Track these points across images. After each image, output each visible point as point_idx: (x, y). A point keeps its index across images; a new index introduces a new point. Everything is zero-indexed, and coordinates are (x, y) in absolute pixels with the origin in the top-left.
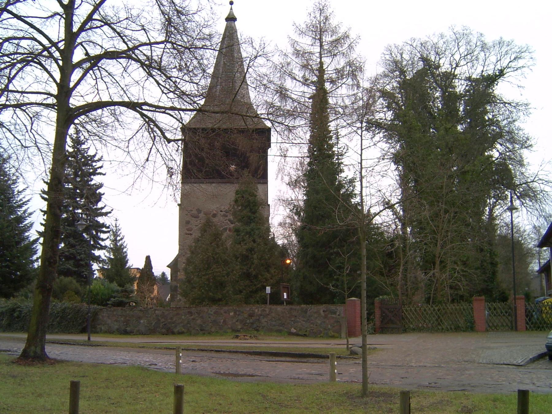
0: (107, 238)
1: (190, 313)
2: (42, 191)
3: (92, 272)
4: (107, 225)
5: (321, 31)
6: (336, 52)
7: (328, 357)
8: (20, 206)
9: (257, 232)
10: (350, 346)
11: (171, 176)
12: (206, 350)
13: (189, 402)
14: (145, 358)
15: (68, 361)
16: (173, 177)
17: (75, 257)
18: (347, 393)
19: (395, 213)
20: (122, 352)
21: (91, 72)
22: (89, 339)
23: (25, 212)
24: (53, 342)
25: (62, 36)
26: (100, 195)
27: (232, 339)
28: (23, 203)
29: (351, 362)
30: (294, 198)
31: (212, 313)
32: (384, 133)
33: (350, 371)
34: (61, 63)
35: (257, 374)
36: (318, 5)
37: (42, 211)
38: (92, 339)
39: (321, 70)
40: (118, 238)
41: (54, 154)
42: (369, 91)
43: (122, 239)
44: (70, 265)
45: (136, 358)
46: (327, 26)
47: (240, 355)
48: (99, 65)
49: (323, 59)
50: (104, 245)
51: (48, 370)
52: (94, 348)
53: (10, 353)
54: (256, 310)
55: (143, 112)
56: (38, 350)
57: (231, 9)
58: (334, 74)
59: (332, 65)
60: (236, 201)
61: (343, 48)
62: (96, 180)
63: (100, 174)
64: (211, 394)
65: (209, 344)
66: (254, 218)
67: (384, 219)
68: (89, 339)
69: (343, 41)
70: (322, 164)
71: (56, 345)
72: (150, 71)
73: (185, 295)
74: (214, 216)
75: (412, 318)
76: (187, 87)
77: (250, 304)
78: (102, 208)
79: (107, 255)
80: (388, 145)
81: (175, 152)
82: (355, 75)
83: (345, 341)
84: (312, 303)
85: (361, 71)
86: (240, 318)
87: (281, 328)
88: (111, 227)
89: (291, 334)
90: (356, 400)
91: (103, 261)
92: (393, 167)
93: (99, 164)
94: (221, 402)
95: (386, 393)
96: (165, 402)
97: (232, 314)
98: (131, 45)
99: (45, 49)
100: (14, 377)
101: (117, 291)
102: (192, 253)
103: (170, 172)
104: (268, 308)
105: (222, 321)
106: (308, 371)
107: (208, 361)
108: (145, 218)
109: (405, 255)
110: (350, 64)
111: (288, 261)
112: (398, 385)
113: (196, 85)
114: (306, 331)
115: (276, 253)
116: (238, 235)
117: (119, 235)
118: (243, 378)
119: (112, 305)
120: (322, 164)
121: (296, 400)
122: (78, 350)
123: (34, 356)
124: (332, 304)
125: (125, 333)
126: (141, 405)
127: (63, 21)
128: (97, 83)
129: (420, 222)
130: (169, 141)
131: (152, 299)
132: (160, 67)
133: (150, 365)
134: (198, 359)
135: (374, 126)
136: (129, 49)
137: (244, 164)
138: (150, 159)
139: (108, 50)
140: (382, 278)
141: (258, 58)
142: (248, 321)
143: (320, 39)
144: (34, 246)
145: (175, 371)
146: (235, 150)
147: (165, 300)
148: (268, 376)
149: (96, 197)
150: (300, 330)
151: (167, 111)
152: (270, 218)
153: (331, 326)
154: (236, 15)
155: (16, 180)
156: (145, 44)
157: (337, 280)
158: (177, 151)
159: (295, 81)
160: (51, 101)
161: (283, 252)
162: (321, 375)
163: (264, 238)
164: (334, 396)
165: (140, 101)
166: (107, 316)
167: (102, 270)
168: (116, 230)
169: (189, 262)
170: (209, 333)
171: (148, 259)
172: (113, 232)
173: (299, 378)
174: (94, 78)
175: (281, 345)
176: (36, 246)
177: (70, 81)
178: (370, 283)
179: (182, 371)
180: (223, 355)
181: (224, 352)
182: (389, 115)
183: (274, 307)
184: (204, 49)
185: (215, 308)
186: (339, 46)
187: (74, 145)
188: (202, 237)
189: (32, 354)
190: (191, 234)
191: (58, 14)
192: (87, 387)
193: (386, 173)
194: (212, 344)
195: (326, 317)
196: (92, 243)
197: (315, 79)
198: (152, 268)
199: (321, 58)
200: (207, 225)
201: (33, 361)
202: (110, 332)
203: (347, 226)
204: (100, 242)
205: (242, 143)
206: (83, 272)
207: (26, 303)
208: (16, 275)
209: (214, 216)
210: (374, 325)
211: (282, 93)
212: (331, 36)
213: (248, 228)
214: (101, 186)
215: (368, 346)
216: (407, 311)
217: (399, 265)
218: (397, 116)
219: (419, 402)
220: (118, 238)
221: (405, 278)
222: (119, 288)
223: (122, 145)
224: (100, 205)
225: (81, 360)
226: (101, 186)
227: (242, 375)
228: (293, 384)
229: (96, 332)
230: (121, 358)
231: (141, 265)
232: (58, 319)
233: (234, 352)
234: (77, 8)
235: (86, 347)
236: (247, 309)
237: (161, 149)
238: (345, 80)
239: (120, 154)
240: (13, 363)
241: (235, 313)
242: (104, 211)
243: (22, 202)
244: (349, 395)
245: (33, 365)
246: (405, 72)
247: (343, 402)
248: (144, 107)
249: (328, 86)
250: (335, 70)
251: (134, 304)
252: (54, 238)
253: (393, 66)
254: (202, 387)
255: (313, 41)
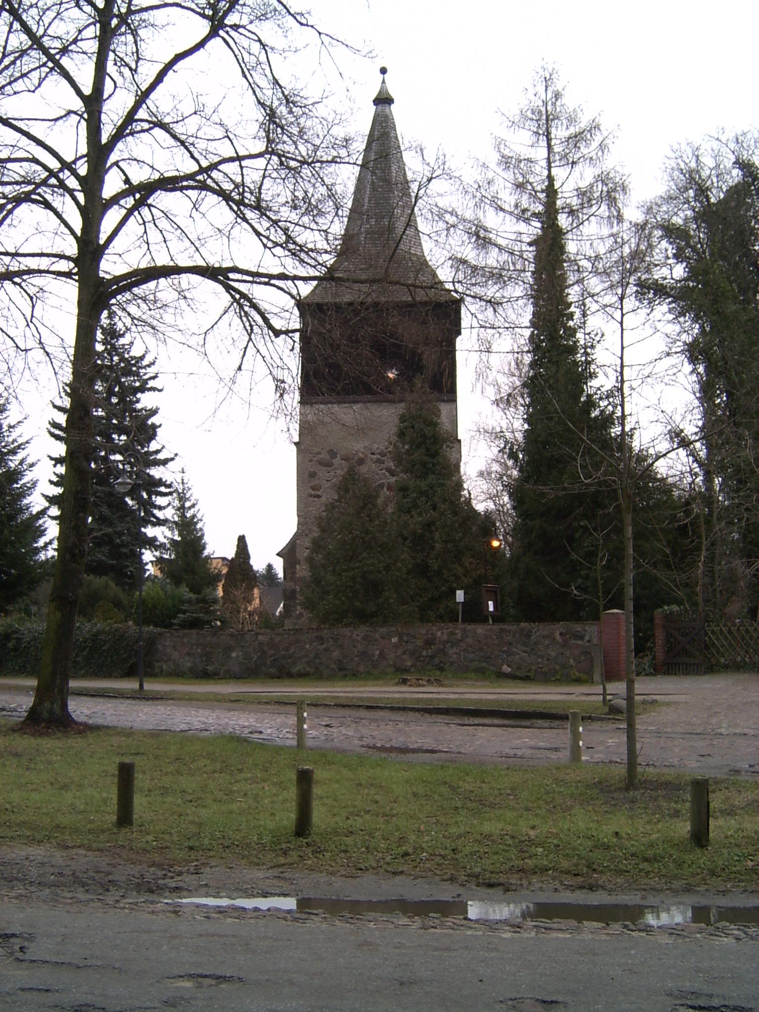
0: (169, 505)
1: (321, 639)
2: (50, 423)
3: (141, 566)
4: (168, 483)
5: (547, 120)
6: (577, 156)
7: (564, 718)
8: (14, 452)
9: (439, 490)
10: (609, 697)
11: (282, 395)
12: (349, 706)
13: (321, 798)
14: (241, 721)
15: (108, 727)
16: (286, 396)
17: (111, 541)
18: (600, 782)
19: (693, 454)
20: (201, 711)
21: (136, 213)
22: (141, 686)
23: (22, 462)
24: (80, 693)
25: (83, 149)
26: (154, 427)
27: (397, 684)
28: (19, 447)
29: (611, 726)
30: (505, 426)
31: (359, 638)
32: (670, 303)
33: (604, 745)
34: (81, 197)
35: (440, 748)
36: (541, 72)
37: (51, 459)
38: (147, 686)
39: (551, 192)
40: (188, 504)
41: (74, 363)
42: (640, 228)
43: (193, 506)
44: (102, 555)
45: (226, 720)
46: (558, 110)
47: (411, 714)
48: (149, 202)
49: (554, 172)
50: (162, 517)
51: (76, 742)
52: (150, 702)
53: (5, 713)
54: (439, 633)
55: (231, 283)
56: (57, 708)
57: (384, 82)
58: (575, 198)
59: (570, 182)
60: (401, 434)
61: (591, 149)
62: (146, 400)
63: (153, 389)
64: (361, 785)
65: (354, 695)
66: (434, 465)
67: (675, 466)
68: (141, 686)
69: (589, 136)
70: (555, 370)
71: (83, 698)
72: (239, 209)
73: (310, 605)
74: (361, 462)
75: (723, 646)
76: (305, 237)
77: (429, 621)
78: (157, 452)
79: (169, 534)
80: (677, 328)
81: (287, 352)
82: (615, 198)
83: (599, 689)
84: (540, 620)
85: (624, 189)
86: (410, 647)
87: (484, 664)
88: (175, 485)
89: (501, 676)
90: (615, 795)
91: (162, 545)
92: (688, 368)
93: (151, 371)
94: (378, 797)
95: (670, 783)
96: (281, 798)
97: (394, 640)
98: (205, 164)
99: (52, 174)
100: (16, 755)
101: (190, 601)
102: (323, 530)
103: (281, 389)
104: (459, 628)
105: (378, 652)
106: (532, 743)
107: (354, 725)
108: (236, 470)
109: (709, 529)
110: (603, 179)
111: (495, 544)
112: (695, 768)
113: (324, 235)
114: (530, 671)
115: (474, 528)
116: (404, 497)
117: (188, 499)
118: (416, 755)
119: (180, 625)
120: (555, 370)
121: (509, 795)
122: (123, 706)
123: (49, 718)
124: (576, 620)
125: (205, 675)
126: (239, 804)
127: (84, 124)
128: (145, 232)
129: (738, 470)
130: (277, 333)
131: (251, 614)
132: (259, 199)
133: (251, 733)
134: (333, 722)
135: (653, 290)
136: (202, 170)
137: (411, 366)
138: (243, 367)
139: (166, 175)
140: (670, 572)
141: (433, 180)
142: (424, 653)
143: (548, 135)
144: (41, 522)
145: (294, 743)
146: (399, 347)
147: (274, 614)
148: (460, 753)
149: (146, 432)
150: (519, 668)
151: (272, 282)
152: (462, 464)
153: (574, 660)
154: (393, 93)
155: (4, 405)
156: (231, 160)
157: (587, 577)
158: (292, 350)
159: (501, 214)
160: (64, 266)
161: (486, 525)
162: (556, 749)
163: (452, 503)
164: (577, 787)
165: (225, 265)
166: (173, 646)
167: (159, 561)
168: (184, 489)
169: (317, 546)
170: (354, 675)
171: (242, 540)
172: (179, 494)
173: (515, 756)
174: (141, 222)
175: (483, 697)
176: (44, 522)
177: (98, 232)
178: (643, 582)
179: (309, 743)
180: (380, 714)
181: (382, 708)
182: (680, 271)
183: (470, 627)
184: (336, 162)
185: (362, 630)
186: (582, 145)
187: (106, 339)
188: (339, 500)
189: (45, 715)
190: (319, 497)
191: (75, 113)
192: (144, 773)
193: (674, 378)
194: (360, 695)
195: (565, 644)
196: (142, 514)
197: (540, 208)
198: (249, 557)
199: (549, 168)
200: (350, 482)
201: (49, 728)
202: (177, 674)
203: (600, 484)
204: (156, 512)
205: (408, 331)
206: (127, 567)
207: (28, 625)
208: (8, 574)
209: (361, 462)
210: (654, 658)
211: (481, 238)
212: (567, 128)
213: (423, 485)
214: (154, 412)
215: (637, 698)
216: (713, 632)
217: (700, 549)
218: (693, 274)
219: (728, 798)
220: (188, 504)
221: (710, 573)
222: (192, 595)
223: (193, 341)
224: (154, 446)
225: (129, 724)
226: (154, 412)
227: (414, 751)
228: (505, 766)
229: (153, 674)
230: (200, 721)
231: (230, 553)
232: (85, 653)
233: (399, 709)
234: (108, 99)
235: (137, 702)
236: (422, 631)
237: (263, 351)
238: (594, 208)
239: (191, 360)
240: (14, 730)
241: (401, 638)
242: (161, 456)
243: (16, 444)
244: (602, 787)
245: (48, 735)
246: (708, 189)
247: (592, 799)
248: (231, 276)
249: (563, 220)
250: (577, 190)
251: (219, 623)
252: (79, 512)
253: (682, 180)
254: (344, 771)
255: (534, 139)
